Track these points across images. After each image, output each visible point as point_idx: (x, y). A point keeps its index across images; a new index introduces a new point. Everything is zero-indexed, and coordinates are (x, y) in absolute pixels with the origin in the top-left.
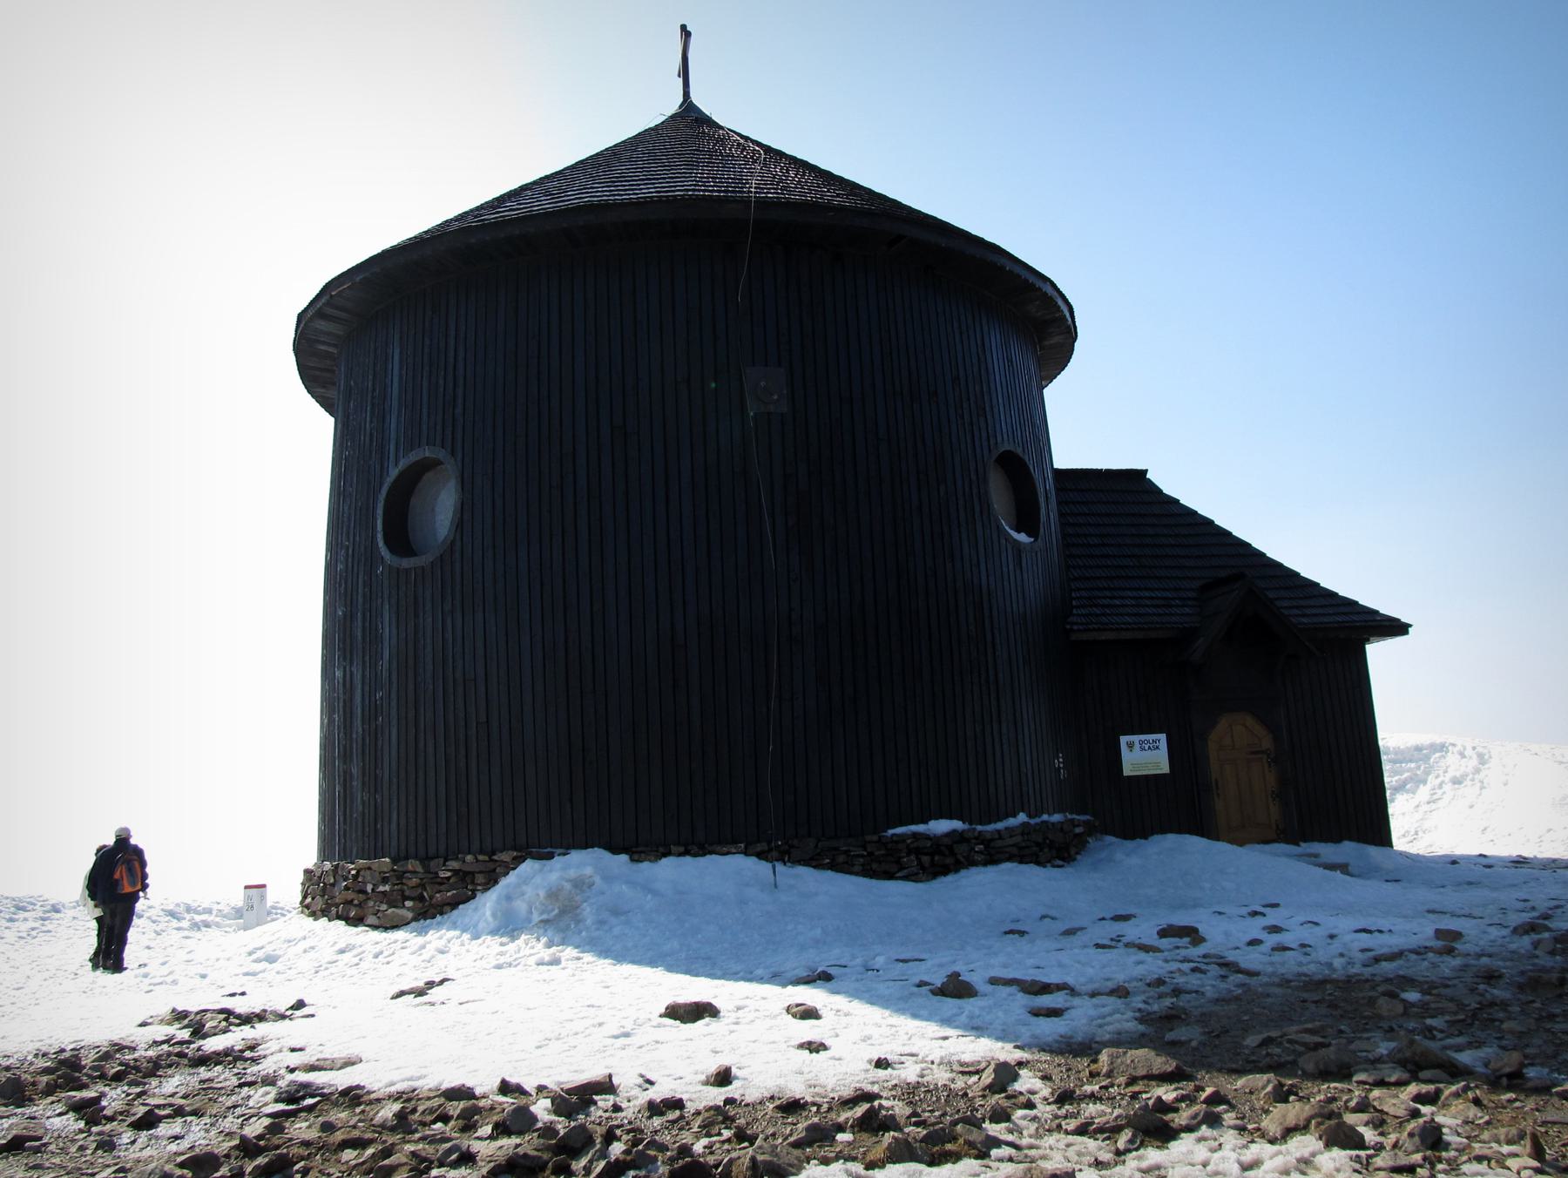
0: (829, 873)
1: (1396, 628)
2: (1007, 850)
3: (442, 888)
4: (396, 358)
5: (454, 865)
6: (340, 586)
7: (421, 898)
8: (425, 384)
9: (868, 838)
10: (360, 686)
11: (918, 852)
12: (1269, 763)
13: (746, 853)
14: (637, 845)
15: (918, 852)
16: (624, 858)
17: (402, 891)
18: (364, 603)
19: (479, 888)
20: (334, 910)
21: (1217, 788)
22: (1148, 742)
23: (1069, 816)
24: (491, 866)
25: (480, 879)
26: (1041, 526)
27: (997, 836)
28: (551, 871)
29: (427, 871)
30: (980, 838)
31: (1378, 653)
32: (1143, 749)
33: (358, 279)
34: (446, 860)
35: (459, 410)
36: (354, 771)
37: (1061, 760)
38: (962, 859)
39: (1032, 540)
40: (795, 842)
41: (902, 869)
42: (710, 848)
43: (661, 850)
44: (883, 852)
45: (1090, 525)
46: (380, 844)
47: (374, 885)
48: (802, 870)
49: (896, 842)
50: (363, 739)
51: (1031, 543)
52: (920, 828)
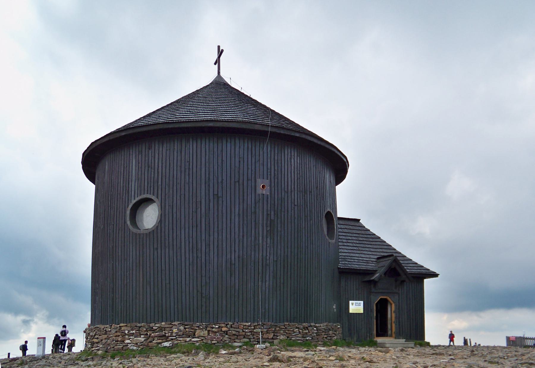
2: (322, 330)
9: (286, 323)
22: (358, 303)
31: (427, 282)
32: (356, 305)
45: (343, 236)
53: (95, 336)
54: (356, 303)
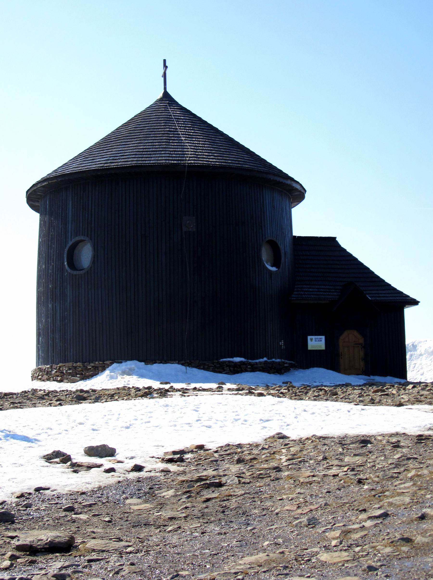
0: (202, 370)
1: (414, 302)
2: (259, 368)
3: (89, 371)
4: (70, 205)
5: (92, 364)
6: (50, 278)
7: (82, 374)
8: (81, 215)
9: (215, 361)
10: (59, 310)
11: (229, 366)
12: (362, 348)
13: (178, 363)
14: (147, 360)
15: (229, 366)
16: (143, 363)
17: (76, 372)
18: (60, 284)
19: (100, 371)
20: (52, 379)
21: (341, 355)
22: (318, 339)
23: (283, 360)
24: (103, 365)
25: (100, 369)
26: (282, 264)
27: (255, 364)
28: (122, 366)
29: (84, 366)
30: (250, 364)
33: (59, 180)
34: (90, 363)
35: (93, 225)
36: (57, 337)
37: (283, 343)
38: (244, 370)
39: (277, 269)
40: (193, 361)
41: (224, 371)
42: (168, 362)
43: (154, 362)
44: (219, 366)
46: (66, 359)
47: (66, 371)
48: (195, 369)
49: (223, 363)
50: (60, 327)
51: (277, 270)
52: (231, 359)
53: (38, 377)
54: (316, 338)
